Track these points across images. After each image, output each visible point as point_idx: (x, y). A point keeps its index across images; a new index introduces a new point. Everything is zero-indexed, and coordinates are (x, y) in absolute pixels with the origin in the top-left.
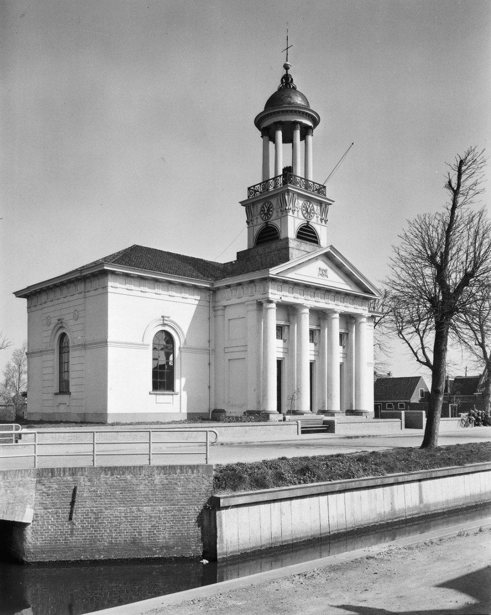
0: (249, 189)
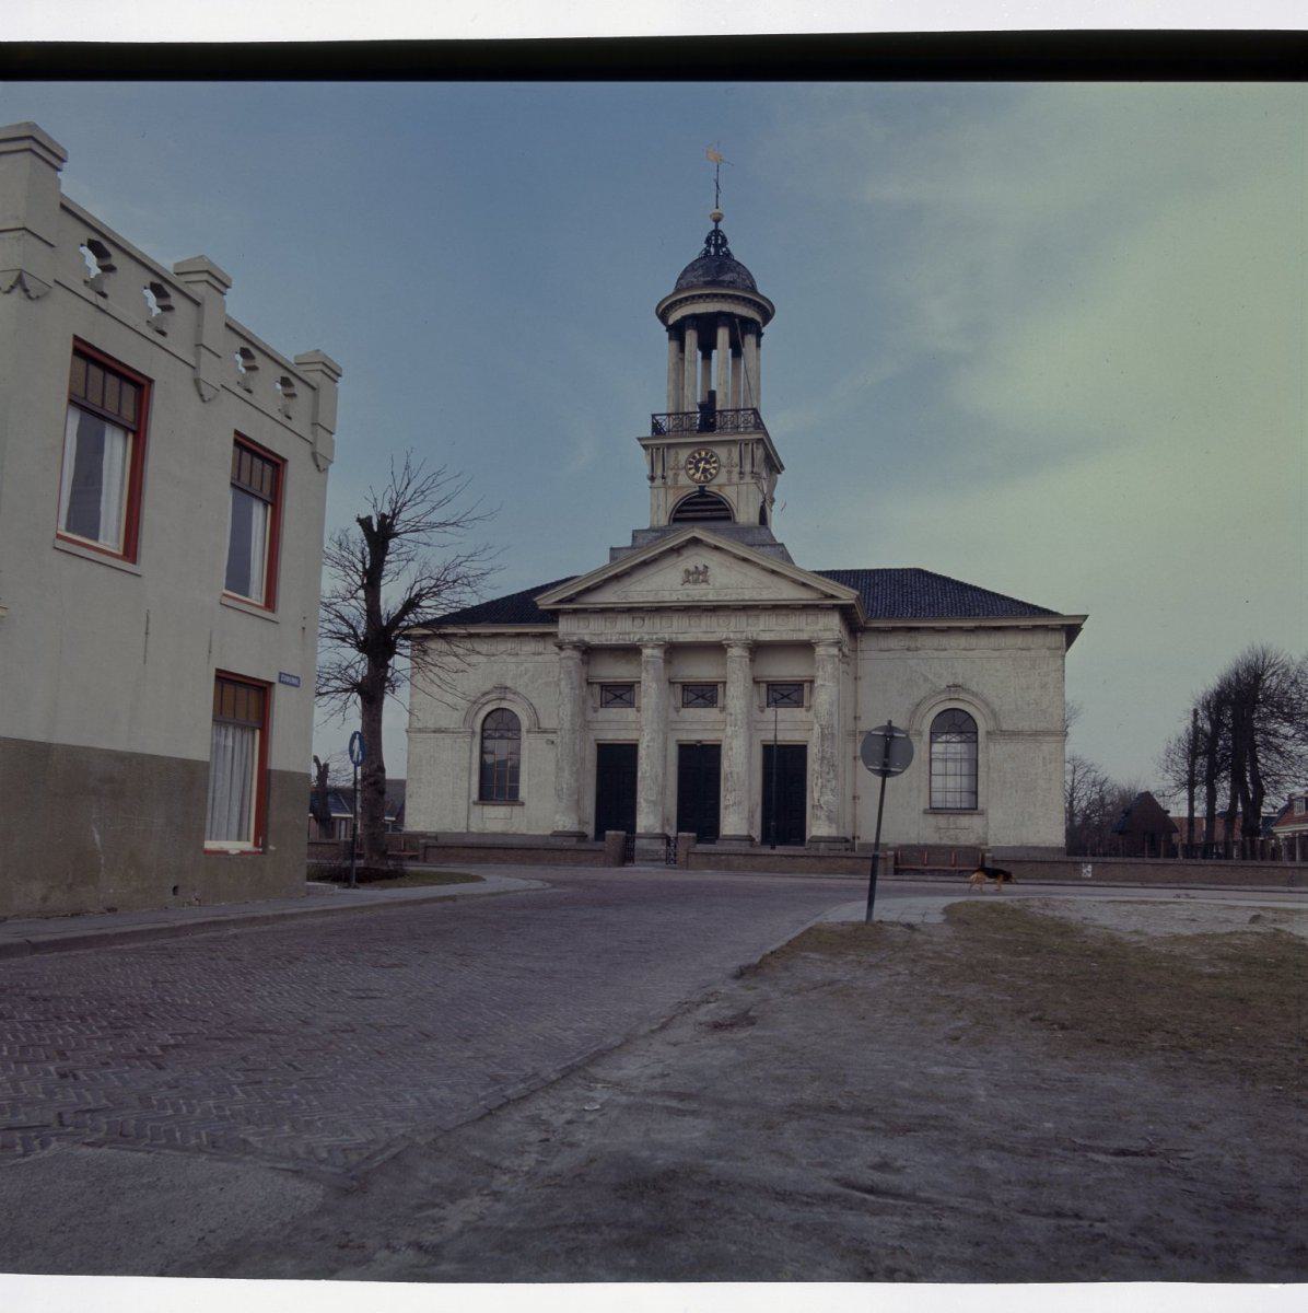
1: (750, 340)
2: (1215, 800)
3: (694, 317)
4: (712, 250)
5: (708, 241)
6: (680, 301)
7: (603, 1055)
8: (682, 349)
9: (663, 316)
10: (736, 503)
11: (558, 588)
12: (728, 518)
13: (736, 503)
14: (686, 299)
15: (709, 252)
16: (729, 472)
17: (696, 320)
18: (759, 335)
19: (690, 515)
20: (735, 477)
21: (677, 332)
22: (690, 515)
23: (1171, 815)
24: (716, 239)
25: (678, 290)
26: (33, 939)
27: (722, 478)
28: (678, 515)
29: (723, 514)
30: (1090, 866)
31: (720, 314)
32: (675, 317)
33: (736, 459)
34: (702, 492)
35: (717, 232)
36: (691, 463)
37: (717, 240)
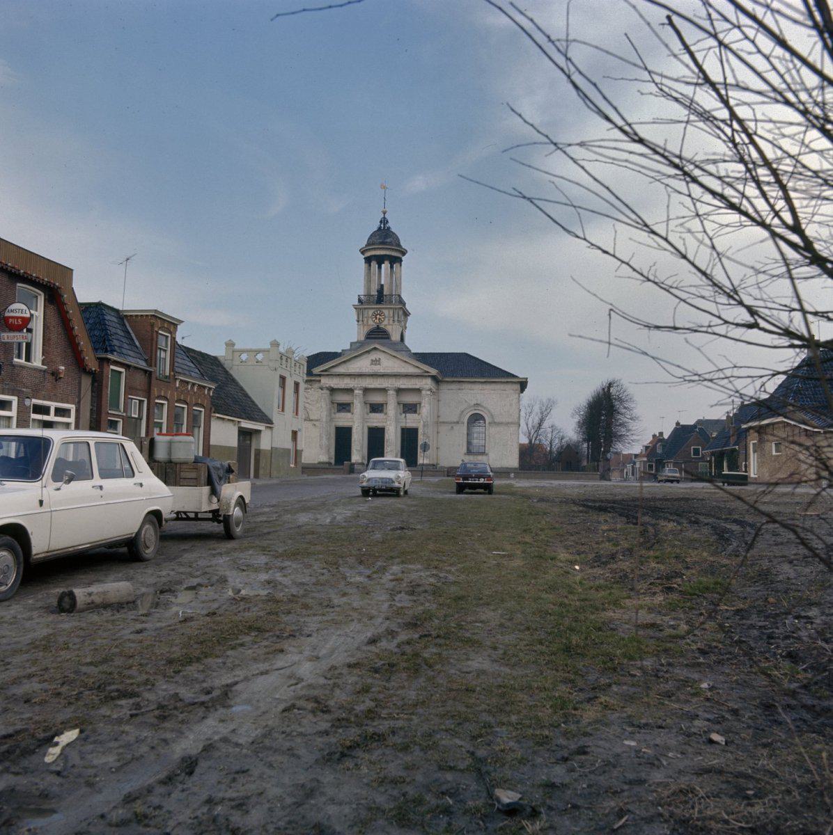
3: (375, 256)
8: (370, 265)
18: (401, 261)
20: (391, 322)
21: (368, 260)
24: (384, 221)
25: (368, 244)
27: (386, 322)
31: (386, 255)
35: (384, 218)
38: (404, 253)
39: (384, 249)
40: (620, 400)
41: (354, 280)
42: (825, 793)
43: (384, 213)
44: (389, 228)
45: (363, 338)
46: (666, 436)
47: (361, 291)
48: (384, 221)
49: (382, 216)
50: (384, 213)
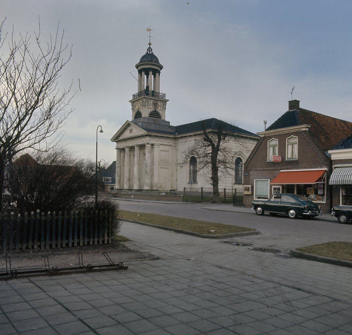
0: (165, 94)
1: (157, 74)
2: (212, 169)
3: (152, 68)
4: (149, 52)
5: (148, 50)
6: (140, 65)
7: (131, 251)
8: (141, 75)
9: (137, 67)
10: (161, 114)
11: (294, 151)
12: (160, 118)
13: (161, 114)
14: (142, 64)
15: (148, 52)
16: (160, 107)
17: (144, 69)
18: (159, 73)
19: (138, 116)
20: (161, 108)
21: (140, 72)
22: (138, 116)
23: (106, 168)
24: (150, 49)
25: (140, 62)
26: (153, 253)
27: (159, 108)
28: (136, 117)
29: (159, 117)
30: (277, 190)
31: (150, 68)
32: (139, 68)
33: (162, 105)
34: (155, 111)
35: (150, 47)
36: (153, 104)
37: (150, 49)
38: (161, 67)
39: (149, 66)
40: (56, 155)
41: (132, 85)
42: (30, 217)
43: (150, 44)
44: (152, 53)
45: (133, 119)
46: (106, 168)
47: (136, 91)
48: (150, 49)
49: (149, 46)
50: (150, 44)
